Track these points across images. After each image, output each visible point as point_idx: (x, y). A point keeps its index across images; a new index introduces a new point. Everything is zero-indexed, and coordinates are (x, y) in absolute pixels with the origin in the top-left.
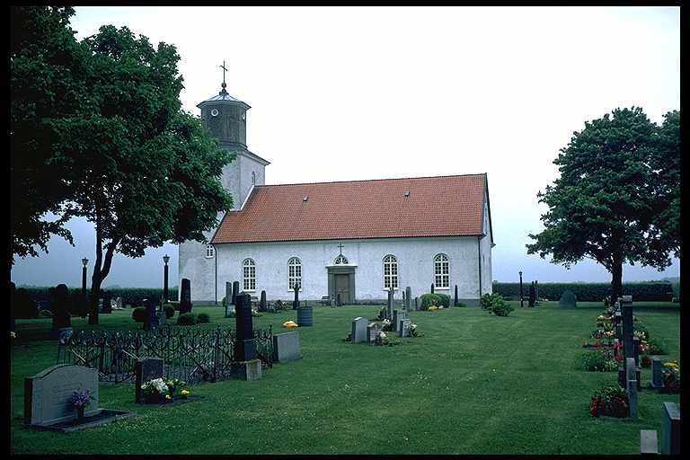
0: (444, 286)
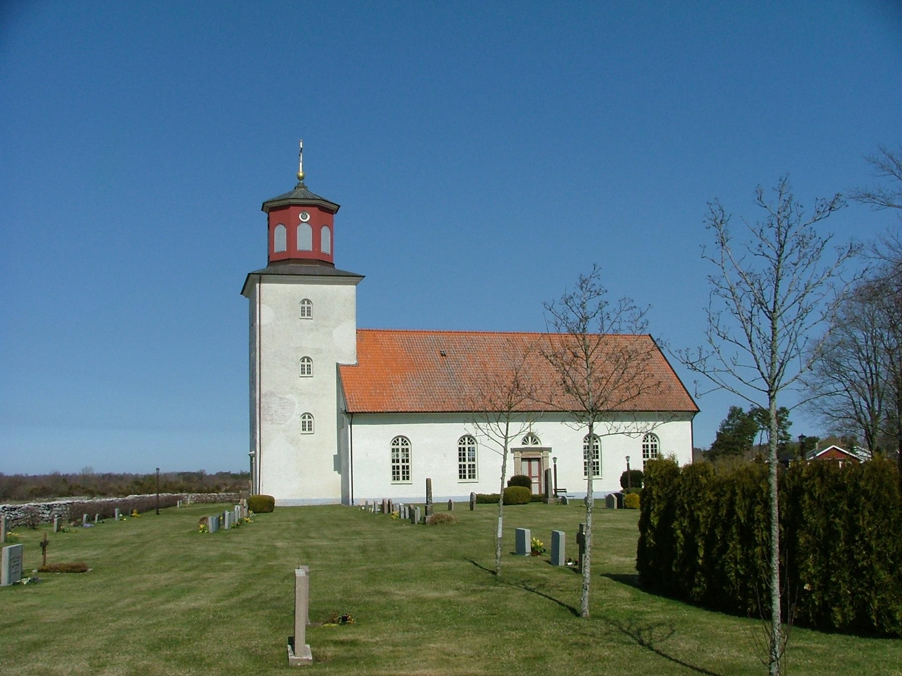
0: (470, 477)
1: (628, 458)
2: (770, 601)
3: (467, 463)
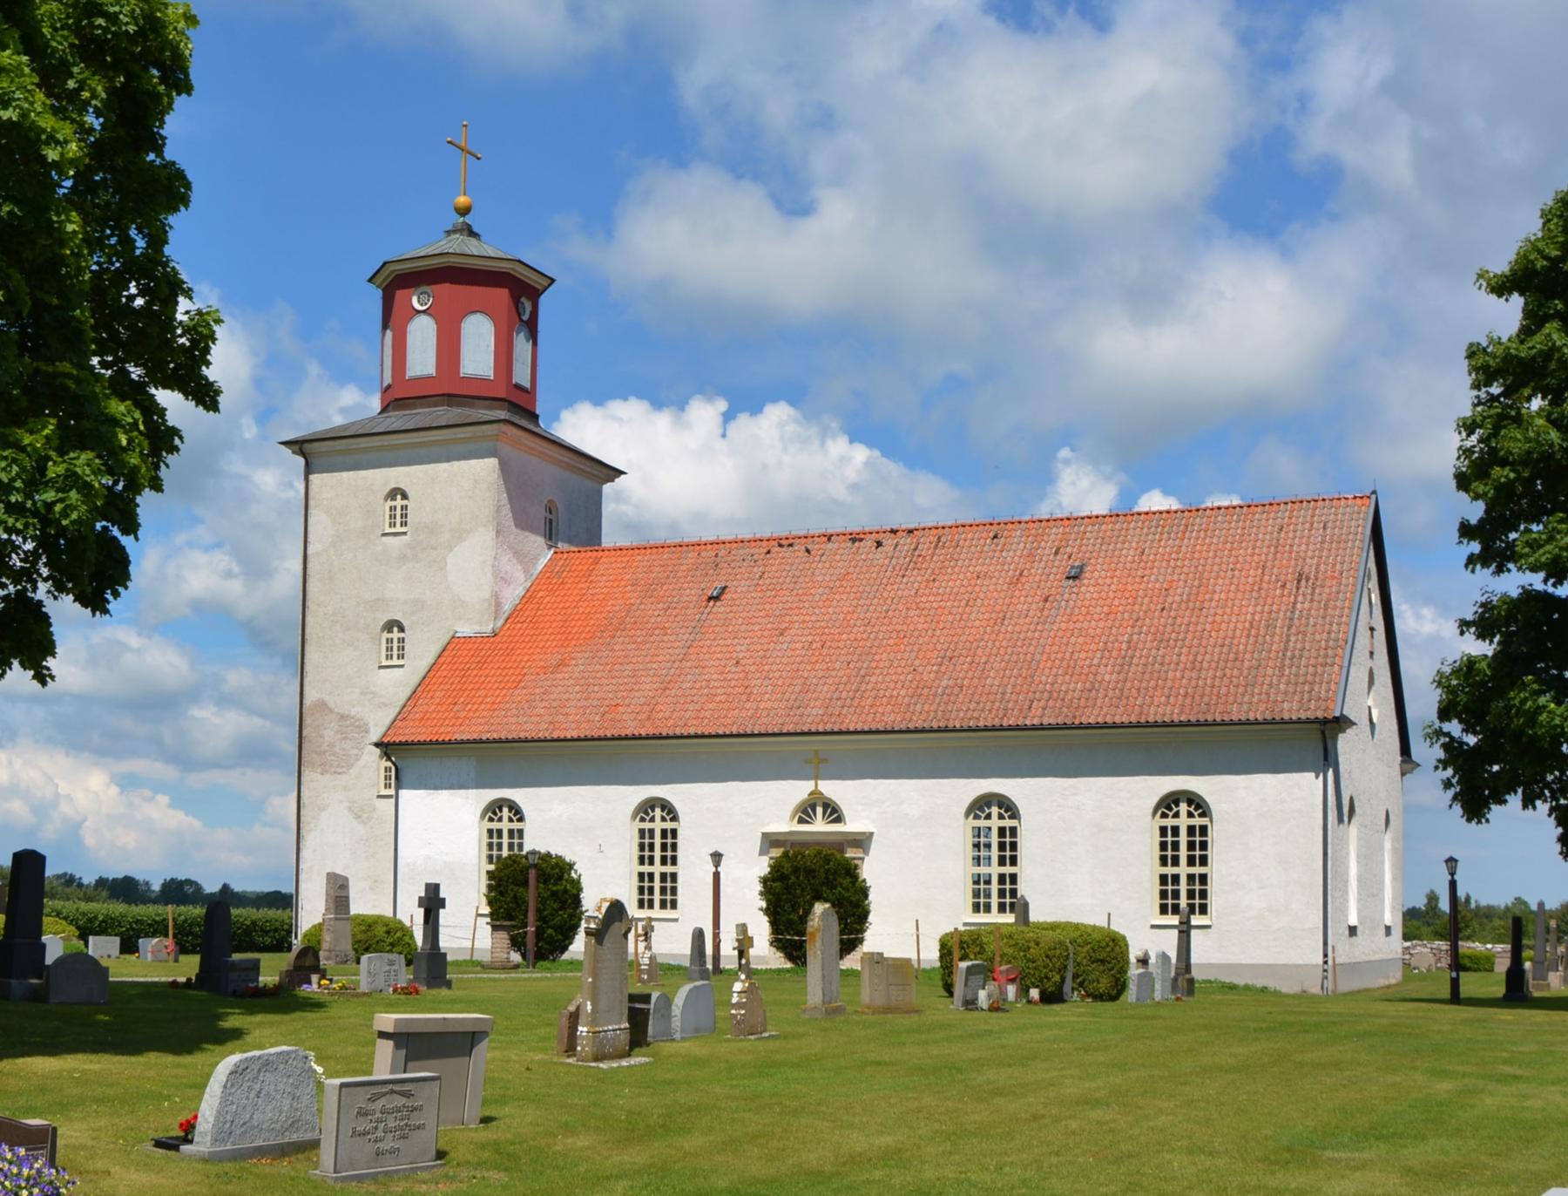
0: (663, 905)
1: (717, 857)
2: (1382, 890)
3: (1183, 870)
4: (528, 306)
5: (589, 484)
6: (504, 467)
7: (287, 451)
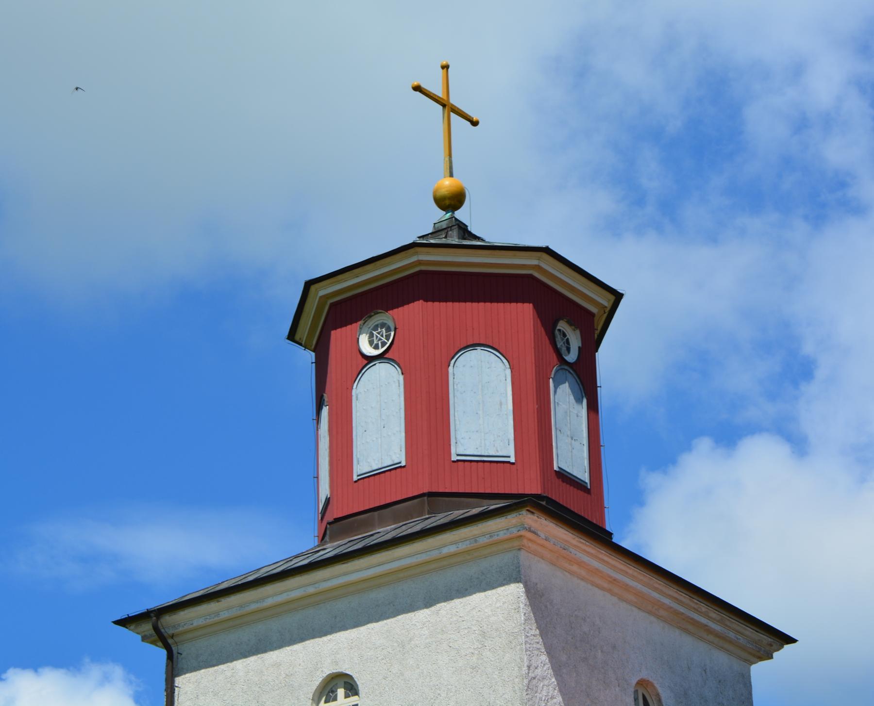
1: (445, 67)
4: (575, 341)
5: (722, 660)
6: (537, 598)
7: (130, 637)
